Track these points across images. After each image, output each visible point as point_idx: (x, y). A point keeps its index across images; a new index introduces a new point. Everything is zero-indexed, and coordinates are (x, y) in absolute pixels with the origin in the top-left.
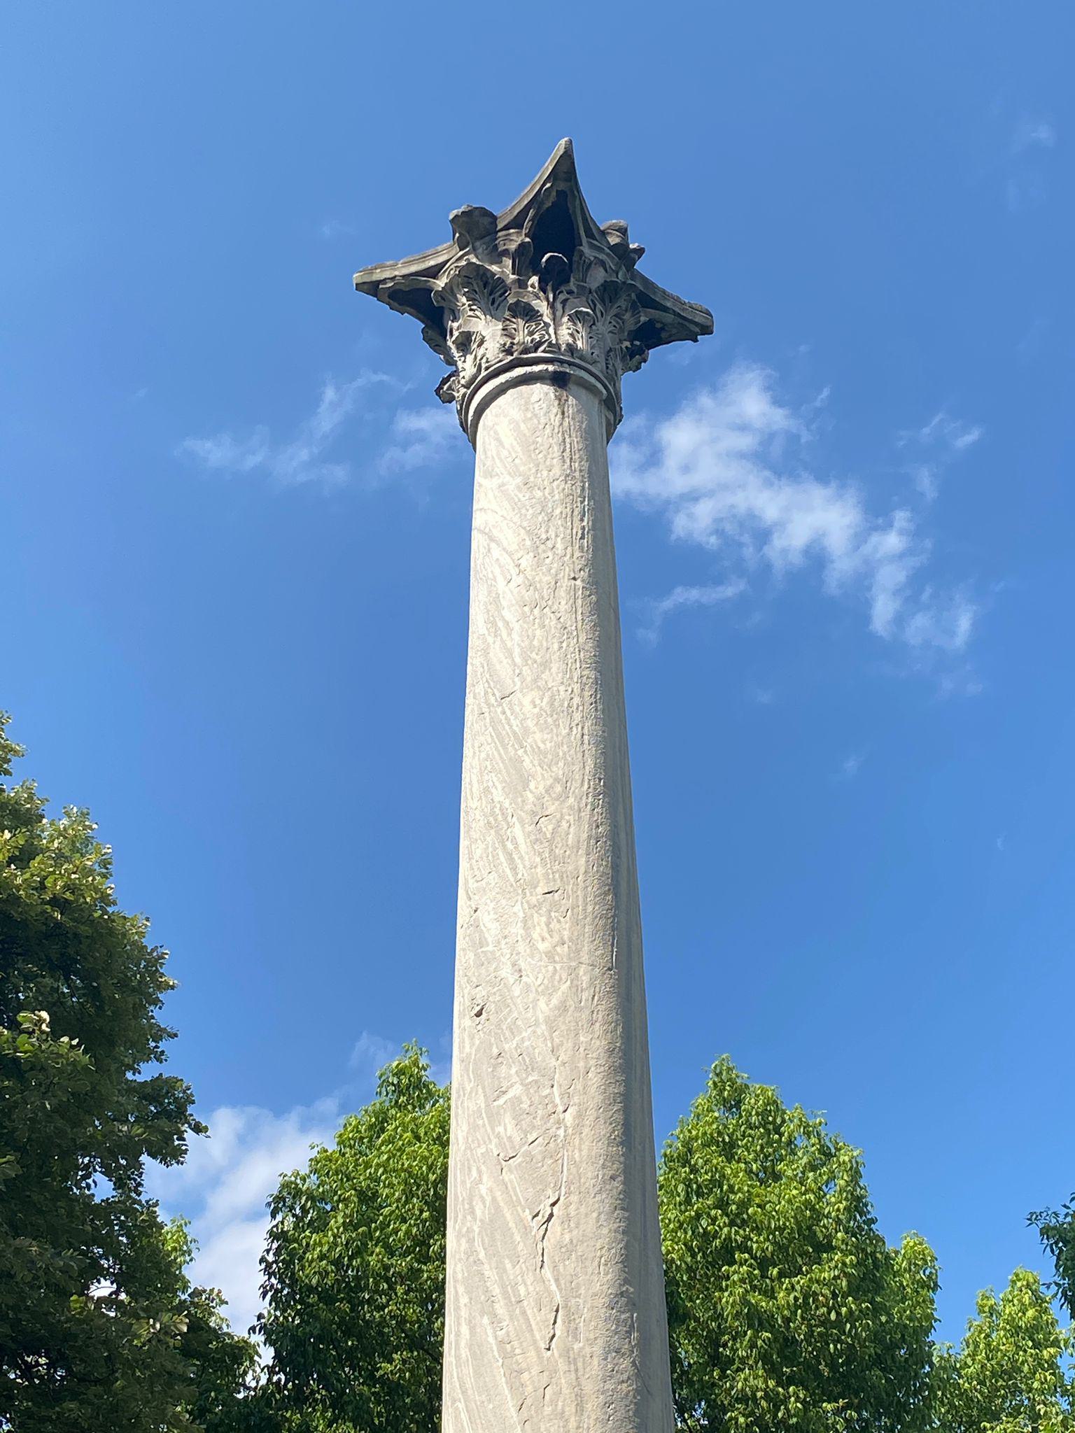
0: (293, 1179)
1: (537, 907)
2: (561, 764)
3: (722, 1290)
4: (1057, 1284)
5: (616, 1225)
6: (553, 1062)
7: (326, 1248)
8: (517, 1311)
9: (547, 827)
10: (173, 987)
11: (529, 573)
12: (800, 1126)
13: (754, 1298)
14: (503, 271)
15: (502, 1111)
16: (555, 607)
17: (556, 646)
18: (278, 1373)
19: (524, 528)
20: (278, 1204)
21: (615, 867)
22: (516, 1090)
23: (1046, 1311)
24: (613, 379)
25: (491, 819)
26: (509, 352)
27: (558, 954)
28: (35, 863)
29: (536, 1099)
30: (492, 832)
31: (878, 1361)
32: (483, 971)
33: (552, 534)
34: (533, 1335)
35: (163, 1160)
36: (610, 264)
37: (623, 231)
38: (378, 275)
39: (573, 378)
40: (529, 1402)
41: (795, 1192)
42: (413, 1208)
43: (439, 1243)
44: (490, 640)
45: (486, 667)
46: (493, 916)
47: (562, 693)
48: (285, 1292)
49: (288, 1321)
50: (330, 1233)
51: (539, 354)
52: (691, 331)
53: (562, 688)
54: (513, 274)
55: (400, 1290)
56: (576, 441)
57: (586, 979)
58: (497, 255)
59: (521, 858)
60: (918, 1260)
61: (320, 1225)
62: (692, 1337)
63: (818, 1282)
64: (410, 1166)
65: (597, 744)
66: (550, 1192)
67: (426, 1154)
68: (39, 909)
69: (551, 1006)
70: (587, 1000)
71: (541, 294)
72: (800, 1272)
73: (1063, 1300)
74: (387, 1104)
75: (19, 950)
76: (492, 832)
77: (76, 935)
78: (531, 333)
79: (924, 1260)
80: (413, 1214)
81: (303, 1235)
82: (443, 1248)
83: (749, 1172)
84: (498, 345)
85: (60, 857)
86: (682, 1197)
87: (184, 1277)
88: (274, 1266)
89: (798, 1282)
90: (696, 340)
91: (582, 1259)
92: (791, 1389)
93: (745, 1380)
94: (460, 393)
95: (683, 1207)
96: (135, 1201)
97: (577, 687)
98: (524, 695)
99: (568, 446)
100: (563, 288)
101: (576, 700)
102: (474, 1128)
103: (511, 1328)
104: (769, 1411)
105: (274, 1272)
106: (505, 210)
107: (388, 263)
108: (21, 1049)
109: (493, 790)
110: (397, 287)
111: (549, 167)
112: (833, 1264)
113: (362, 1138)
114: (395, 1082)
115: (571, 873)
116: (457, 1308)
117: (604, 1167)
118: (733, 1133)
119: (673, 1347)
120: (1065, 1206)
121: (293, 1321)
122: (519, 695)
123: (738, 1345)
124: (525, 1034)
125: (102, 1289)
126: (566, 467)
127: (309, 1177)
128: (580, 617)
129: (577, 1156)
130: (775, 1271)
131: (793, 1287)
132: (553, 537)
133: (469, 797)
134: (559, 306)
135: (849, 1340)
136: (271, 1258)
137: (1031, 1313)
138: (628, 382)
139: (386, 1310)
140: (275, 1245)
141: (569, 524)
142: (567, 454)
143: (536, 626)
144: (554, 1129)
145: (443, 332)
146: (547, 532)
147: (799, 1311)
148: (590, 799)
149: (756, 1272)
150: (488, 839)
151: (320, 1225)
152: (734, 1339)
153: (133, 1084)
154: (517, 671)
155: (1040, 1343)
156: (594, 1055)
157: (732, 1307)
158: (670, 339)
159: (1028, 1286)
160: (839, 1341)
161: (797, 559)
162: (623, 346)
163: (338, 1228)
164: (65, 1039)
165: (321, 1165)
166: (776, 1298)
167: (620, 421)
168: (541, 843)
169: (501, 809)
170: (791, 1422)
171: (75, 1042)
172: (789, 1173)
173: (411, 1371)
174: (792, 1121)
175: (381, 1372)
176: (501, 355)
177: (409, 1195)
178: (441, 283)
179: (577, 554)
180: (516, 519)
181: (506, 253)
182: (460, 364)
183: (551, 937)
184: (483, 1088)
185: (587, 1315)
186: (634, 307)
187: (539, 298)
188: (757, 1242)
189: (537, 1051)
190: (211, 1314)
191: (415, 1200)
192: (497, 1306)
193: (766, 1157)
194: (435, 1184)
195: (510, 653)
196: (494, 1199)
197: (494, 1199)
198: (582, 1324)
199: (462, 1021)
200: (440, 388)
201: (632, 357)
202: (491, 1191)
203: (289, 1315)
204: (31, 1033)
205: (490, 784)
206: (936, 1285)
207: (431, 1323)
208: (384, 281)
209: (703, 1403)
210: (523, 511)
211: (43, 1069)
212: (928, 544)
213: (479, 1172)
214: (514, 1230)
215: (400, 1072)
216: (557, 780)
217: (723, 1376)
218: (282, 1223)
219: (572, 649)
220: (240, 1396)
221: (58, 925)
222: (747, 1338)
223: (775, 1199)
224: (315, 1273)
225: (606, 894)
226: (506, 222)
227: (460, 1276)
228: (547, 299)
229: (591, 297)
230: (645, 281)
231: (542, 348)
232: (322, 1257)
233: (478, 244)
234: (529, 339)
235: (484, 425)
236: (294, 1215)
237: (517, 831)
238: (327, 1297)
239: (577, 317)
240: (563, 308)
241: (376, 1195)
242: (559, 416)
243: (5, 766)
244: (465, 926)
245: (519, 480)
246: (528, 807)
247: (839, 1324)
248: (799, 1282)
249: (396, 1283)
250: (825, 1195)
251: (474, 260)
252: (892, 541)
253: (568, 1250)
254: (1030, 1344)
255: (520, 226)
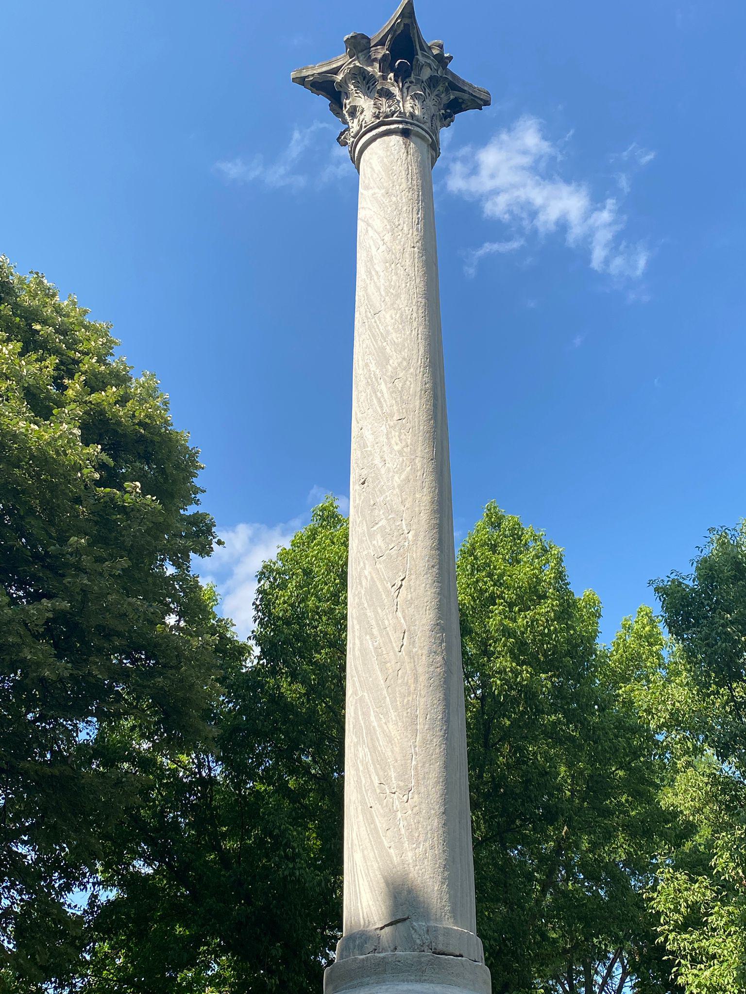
0: (269, 563)
1: (394, 427)
2: (406, 350)
3: (489, 618)
4: (662, 616)
5: (434, 590)
6: (402, 508)
7: (287, 598)
8: (384, 633)
9: (399, 384)
10: (203, 468)
11: (388, 244)
12: (531, 536)
13: (506, 622)
14: (374, 71)
15: (376, 533)
16: (403, 263)
17: (404, 285)
18: (262, 659)
19: (386, 219)
20: (261, 576)
21: (435, 406)
22: (383, 523)
23: (656, 627)
24: (435, 132)
25: (369, 380)
26: (377, 117)
27: (405, 452)
28: (129, 404)
29: (393, 527)
30: (370, 387)
31: (569, 653)
32: (366, 461)
33: (401, 222)
34: (392, 645)
35: (201, 555)
36: (434, 66)
37: (441, 47)
38: (305, 73)
39: (413, 132)
40: (390, 677)
41: (528, 569)
42: (331, 577)
43: (344, 595)
44: (368, 281)
45: (366, 298)
46: (370, 432)
47: (407, 311)
48: (266, 620)
49: (267, 634)
50: (289, 591)
51: (394, 118)
52: (477, 103)
53: (407, 308)
54: (380, 72)
55: (324, 618)
56: (414, 168)
57: (419, 465)
58: (370, 61)
59: (385, 401)
60: (591, 602)
61: (283, 586)
62: (473, 641)
63: (539, 614)
64: (329, 557)
65: (425, 340)
66: (401, 574)
67: (338, 551)
68: (132, 428)
69: (401, 479)
70: (420, 476)
71: (395, 84)
72: (529, 609)
73: (665, 624)
74: (317, 525)
75: (122, 449)
76: (370, 387)
77: (151, 441)
78: (390, 106)
79: (594, 603)
80: (331, 581)
81: (274, 591)
82: (346, 598)
83: (504, 559)
84: (371, 113)
85: (142, 401)
86: (470, 572)
87: (214, 612)
88: (260, 607)
89: (529, 614)
90: (481, 109)
91: (417, 607)
92: (524, 667)
93: (501, 662)
94: (350, 141)
95: (470, 577)
96: (187, 575)
97: (415, 308)
98: (386, 312)
99: (410, 171)
100: (407, 80)
101: (415, 315)
102: (361, 541)
103: (381, 641)
104: (513, 678)
105: (260, 610)
106: (375, 36)
107: (310, 66)
108: (126, 501)
109: (370, 365)
110: (315, 80)
111: (399, 10)
112: (546, 605)
113: (304, 543)
114: (321, 514)
115: (412, 409)
116: (353, 632)
117: (428, 561)
118: (496, 540)
119: (463, 646)
120: (668, 577)
121: (270, 634)
122: (383, 312)
123: (497, 645)
124: (387, 494)
125: (171, 620)
126: (409, 183)
127: (277, 562)
128: (416, 269)
129: (414, 556)
130: (517, 609)
131: (526, 617)
132: (402, 223)
133: (357, 368)
134: (405, 90)
135: (554, 643)
136: (258, 603)
137: (647, 629)
138: (445, 135)
139: (318, 629)
140: (260, 596)
141: (411, 216)
142: (409, 176)
143: (393, 274)
144: (403, 542)
145: (341, 106)
146: (399, 220)
147: (529, 629)
148: (422, 369)
149: (507, 609)
150: (368, 391)
151: (283, 586)
152: (495, 642)
153: (184, 516)
154: (383, 299)
155: (652, 644)
156: (424, 504)
157: (495, 626)
158: (467, 108)
159: (647, 614)
160: (549, 643)
161: (552, 227)
162: (441, 113)
163: (293, 588)
164: (149, 496)
165: (283, 556)
166: (517, 622)
167: (439, 156)
168: (396, 393)
169: (374, 375)
170: (524, 683)
171: (154, 498)
172: (525, 559)
173: (330, 658)
174: (527, 534)
175: (315, 659)
176: (373, 119)
177: (329, 571)
178: (339, 77)
179: (415, 233)
180: (382, 213)
181: (375, 60)
182: (350, 124)
183: (401, 443)
184: (366, 521)
185: (419, 634)
186: (447, 91)
187: (394, 86)
188: (507, 594)
189: (394, 502)
190: (228, 631)
191: (332, 574)
192: (374, 630)
193: (513, 552)
194: (342, 566)
195: (379, 289)
196: (372, 578)
197: (372, 578)
198: (417, 639)
199: (354, 487)
200: (339, 138)
201: (445, 118)
202: (370, 574)
203: (268, 631)
204: (131, 493)
205: (369, 361)
206: (600, 614)
207: (340, 635)
208: (308, 77)
209: (478, 673)
210: (386, 208)
211: (139, 510)
212: (625, 217)
213: (364, 564)
214: (383, 593)
215: (323, 510)
216: (404, 359)
217: (489, 660)
218: (264, 585)
219: (412, 287)
220: (244, 671)
221: (142, 436)
222: (502, 642)
223: (517, 573)
224: (281, 610)
225: (430, 420)
226: (375, 42)
227: (355, 616)
228: (399, 86)
229: (423, 85)
230: (453, 75)
231: (396, 115)
232: (285, 602)
233: (360, 54)
234: (389, 109)
235: (364, 159)
236: (270, 582)
237: (383, 387)
238: (287, 622)
239: (415, 97)
240: (408, 91)
241: (311, 571)
242: (405, 154)
243: (111, 351)
244: (356, 437)
245: (383, 191)
246: (389, 374)
247: (549, 635)
248: (529, 614)
249: (322, 615)
250: (543, 571)
251: (358, 64)
252: (605, 216)
253: (410, 602)
254: (647, 644)
255: (384, 45)
